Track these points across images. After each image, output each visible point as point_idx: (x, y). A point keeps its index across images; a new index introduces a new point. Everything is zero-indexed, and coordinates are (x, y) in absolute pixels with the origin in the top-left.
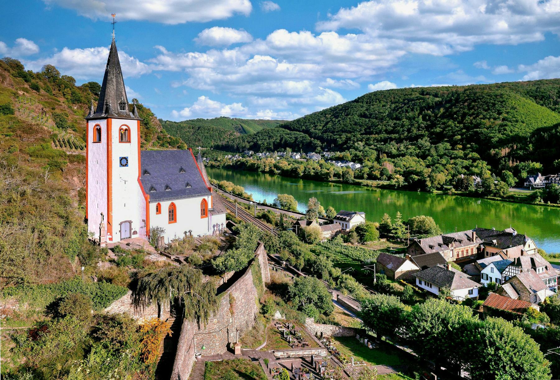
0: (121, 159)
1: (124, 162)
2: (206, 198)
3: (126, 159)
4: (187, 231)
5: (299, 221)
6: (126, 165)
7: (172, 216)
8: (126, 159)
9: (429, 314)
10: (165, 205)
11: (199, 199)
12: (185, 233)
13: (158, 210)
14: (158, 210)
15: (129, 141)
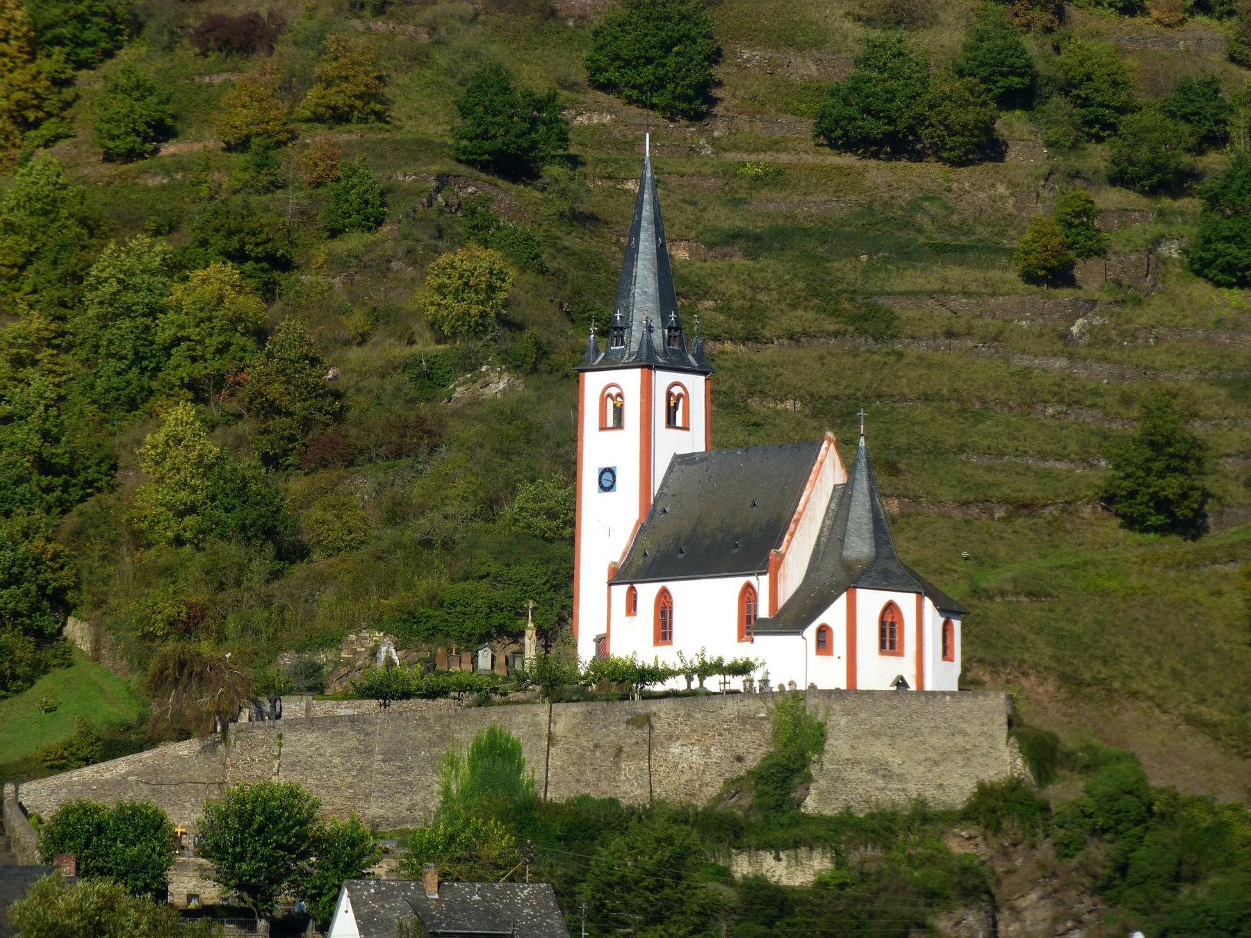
1: (608, 479)
10: (648, 592)
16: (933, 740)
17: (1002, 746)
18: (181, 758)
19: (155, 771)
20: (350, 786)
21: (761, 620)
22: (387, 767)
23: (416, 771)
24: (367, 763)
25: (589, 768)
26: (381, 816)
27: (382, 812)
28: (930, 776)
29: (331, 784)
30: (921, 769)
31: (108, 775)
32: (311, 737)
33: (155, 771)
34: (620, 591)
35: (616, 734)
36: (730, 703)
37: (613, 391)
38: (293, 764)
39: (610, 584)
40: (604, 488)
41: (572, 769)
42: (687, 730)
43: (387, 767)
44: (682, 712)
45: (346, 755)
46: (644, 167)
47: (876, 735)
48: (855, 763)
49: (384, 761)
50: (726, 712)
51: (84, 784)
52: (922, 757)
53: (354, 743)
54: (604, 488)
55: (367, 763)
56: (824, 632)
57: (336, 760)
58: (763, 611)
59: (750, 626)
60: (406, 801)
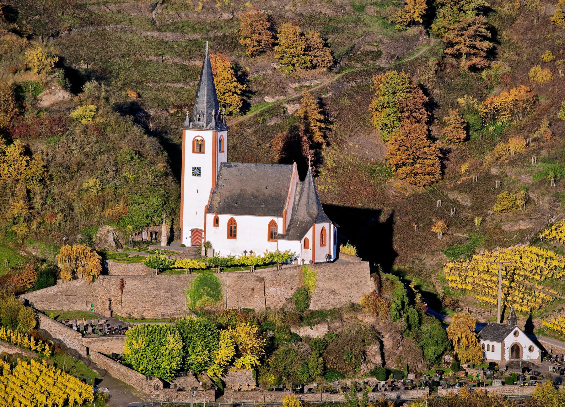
0: (194, 169)
1: (197, 172)
2: (275, 219)
3: (199, 169)
4: (248, 251)
5: (221, 277)
6: (199, 175)
7: (232, 232)
8: (199, 169)
9: (34, 181)
10: (224, 219)
11: (268, 219)
12: (245, 252)
13: (216, 222)
14: (216, 222)
15: (192, 231)
16: (348, 281)
17: (369, 281)
18: (77, 286)
19: (67, 291)
20: (152, 301)
21: (279, 235)
22: (166, 295)
23: (178, 297)
24: (158, 293)
25: (241, 296)
26: (165, 312)
27: (165, 311)
28: (347, 293)
29: (144, 300)
30: (345, 291)
31: (50, 293)
32: (135, 283)
33: (67, 291)
34: (211, 218)
35: (251, 284)
36: (287, 271)
37: (199, 139)
38: (128, 292)
39: (206, 213)
40: (194, 175)
41: (235, 296)
42: (275, 282)
43: (166, 295)
44: (273, 276)
45: (150, 290)
46: (205, 49)
47: (331, 280)
48: (324, 290)
49: (165, 292)
50: (286, 275)
51: (42, 296)
52: (345, 287)
53: (153, 285)
54: (194, 175)
55: (158, 293)
56: (306, 242)
57: (145, 292)
58: (280, 231)
59: (273, 235)
60: (174, 308)
